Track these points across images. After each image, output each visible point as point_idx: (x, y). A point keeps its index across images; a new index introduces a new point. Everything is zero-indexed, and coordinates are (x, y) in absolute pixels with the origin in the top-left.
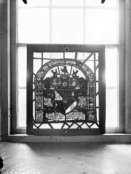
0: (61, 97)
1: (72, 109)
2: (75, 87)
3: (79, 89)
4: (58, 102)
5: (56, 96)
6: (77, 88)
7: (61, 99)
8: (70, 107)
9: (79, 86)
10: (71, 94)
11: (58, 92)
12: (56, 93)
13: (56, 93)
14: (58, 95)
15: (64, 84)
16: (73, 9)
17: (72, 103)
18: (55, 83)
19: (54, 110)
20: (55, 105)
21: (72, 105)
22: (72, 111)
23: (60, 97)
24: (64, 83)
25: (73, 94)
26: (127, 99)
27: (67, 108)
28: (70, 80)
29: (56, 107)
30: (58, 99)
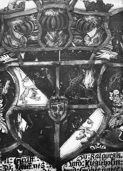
0: (40, 93)
1: (85, 140)
2: (96, 49)
3: (112, 60)
4: (27, 112)
5: (22, 90)
6: (107, 55)
7: (41, 100)
8: (77, 134)
9: (114, 44)
10: (81, 82)
11: (30, 72)
12: (20, 75)
13: (20, 75)
14: (30, 83)
15: (52, 41)
16: (109, 3)
17: (86, 115)
18: (17, 35)
19: (14, 145)
20: (17, 124)
21: (85, 125)
22: (85, 149)
23: (38, 91)
24: (53, 33)
25: (88, 80)
26: (9, 49)
27: (65, 136)
28: (73, 21)
29: (20, 135)
30: (31, 102)
